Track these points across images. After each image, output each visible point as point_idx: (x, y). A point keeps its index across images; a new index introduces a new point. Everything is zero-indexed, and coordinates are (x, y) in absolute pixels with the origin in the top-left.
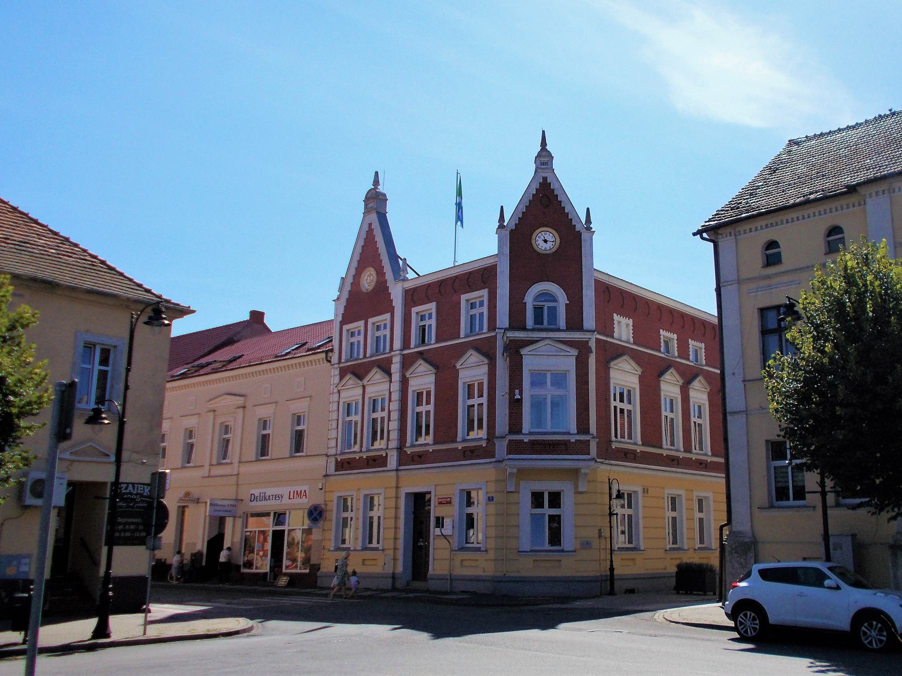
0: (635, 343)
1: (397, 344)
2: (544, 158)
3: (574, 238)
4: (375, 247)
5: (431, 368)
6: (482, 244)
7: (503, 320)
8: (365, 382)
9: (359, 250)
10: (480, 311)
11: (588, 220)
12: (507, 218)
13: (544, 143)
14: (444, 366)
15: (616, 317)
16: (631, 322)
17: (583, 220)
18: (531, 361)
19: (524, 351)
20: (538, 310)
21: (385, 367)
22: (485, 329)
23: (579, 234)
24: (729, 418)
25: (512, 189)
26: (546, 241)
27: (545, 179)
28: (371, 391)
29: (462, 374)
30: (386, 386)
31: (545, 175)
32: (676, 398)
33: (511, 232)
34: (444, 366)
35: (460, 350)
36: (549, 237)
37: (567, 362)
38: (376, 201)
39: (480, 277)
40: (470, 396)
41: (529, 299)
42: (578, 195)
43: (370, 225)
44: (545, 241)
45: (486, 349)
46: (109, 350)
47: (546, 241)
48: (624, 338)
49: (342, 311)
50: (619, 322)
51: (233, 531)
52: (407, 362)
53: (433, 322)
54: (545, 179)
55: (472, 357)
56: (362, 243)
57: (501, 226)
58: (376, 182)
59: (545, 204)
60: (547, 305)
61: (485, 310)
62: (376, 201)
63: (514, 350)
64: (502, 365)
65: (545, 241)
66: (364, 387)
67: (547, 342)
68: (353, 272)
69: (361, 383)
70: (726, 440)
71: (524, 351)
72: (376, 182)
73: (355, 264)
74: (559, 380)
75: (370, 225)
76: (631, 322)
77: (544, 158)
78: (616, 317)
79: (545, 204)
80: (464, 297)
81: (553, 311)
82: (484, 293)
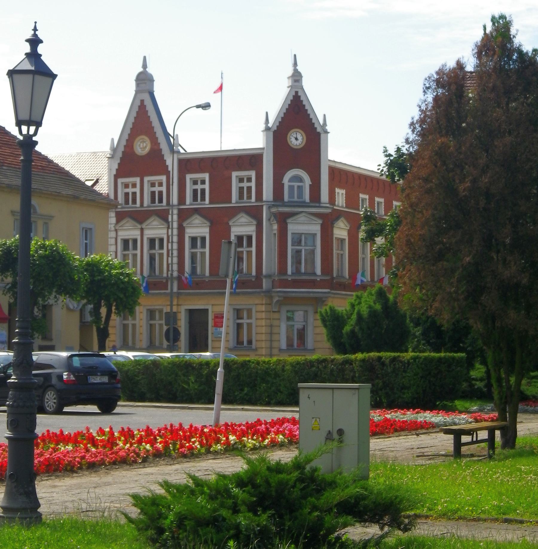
0: (346, 207)
1: (175, 200)
2: (297, 77)
3: (315, 136)
4: (144, 119)
5: (205, 221)
8: (144, 226)
11: (325, 124)
13: (295, 64)
14: (219, 222)
16: (344, 192)
17: (321, 122)
18: (294, 227)
19: (289, 221)
20: (291, 188)
21: (163, 216)
23: (319, 134)
24: (222, 149)
27: (297, 92)
28: (149, 233)
30: (165, 231)
31: (296, 90)
32: (345, 239)
33: (275, 132)
34: (219, 222)
35: (235, 211)
36: (300, 137)
37: (315, 228)
38: (144, 81)
39: (250, 160)
42: (320, 106)
44: (297, 139)
45: (255, 213)
48: (340, 205)
49: (116, 166)
50: (338, 193)
52: (184, 215)
53: (207, 187)
54: (297, 92)
55: (243, 218)
56: (134, 114)
57: (267, 129)
58: (145, 66)
59: (297, 115)
60: (296, 184)
62: (144, 81)
63: (282, 220)
65: (297, 139)
66: (142, 230)
67: (303, 214)
69: (139, 226)
70: (358, 400)
72: (145, 66)
76: (344, 192)
77: (297, 77)
79: (297, 115)
80: (235, 175)
81: (300, 188)
82: (253, 174)
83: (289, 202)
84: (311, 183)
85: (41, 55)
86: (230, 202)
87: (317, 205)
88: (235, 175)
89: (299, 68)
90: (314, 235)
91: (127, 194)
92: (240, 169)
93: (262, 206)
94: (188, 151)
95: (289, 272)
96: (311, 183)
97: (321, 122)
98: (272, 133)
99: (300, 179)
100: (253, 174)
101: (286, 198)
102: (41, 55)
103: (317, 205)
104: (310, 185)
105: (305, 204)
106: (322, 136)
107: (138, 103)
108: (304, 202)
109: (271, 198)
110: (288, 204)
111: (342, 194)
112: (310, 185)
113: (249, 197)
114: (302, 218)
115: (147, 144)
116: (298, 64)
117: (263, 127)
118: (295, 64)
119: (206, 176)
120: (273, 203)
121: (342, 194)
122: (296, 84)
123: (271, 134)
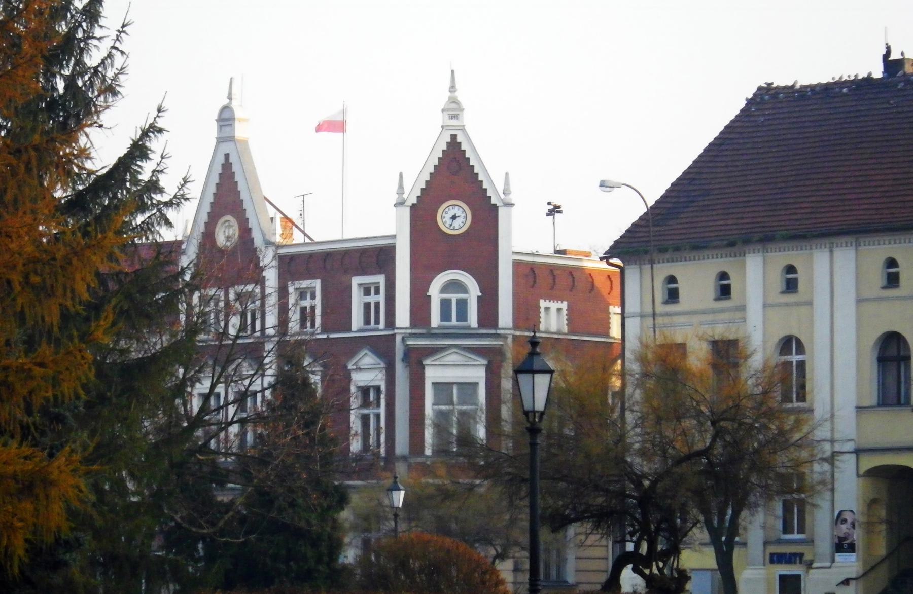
2: (454, 110)
3: (486, 214)
6: (379, 218)
7: (403, 318)
9: (212, 189)
10: (377, 300)
12: (408, 186)
13: (453, 88)
15: (543, 304)
16: (564, 305)
17: (500, 188)
18: (433, 374)
19: (427, 362)
20: (445, 305)
22: (382, 325)
23: (495, 208)
25: (417, 164)
26: (454, 218)
27: (454, 137)
29: (355, 376)
31: (454, 132)
37: (477, 373)
39: (378, 258)
40: (366, 403)
41: (435, 291)
42: (493, 165)
43: (227, 156)
45: (382, 347)
46: (772, 555)
47: (454, 218)
51: (898, 196)
53: (318, 302)
54: (454, 137)
55: (367, 359)
56: (216, 179)
57: (400, 204)
59: (455, 172)
60: (454, 297)
61: (381, 298)
63: (415, 360)
64: (401, 373)
68: (204, 218)
71: (427, 362)
73: (207, 208)
74: (468, 388)
75: (227, 156)
76: (564, 305)
77: (454, 110)
78: (543, 304)
79: (455, 172)
80: (356, 281)
81: (462, 305)
83: (439, 328)
84: (480, 294)
85: (747, 100)
86: (349, 330)
87: (493, 332)
88: (356, 281)
89: (460, 95)
90: (476, 384)
91: (303, 309)
92: (363, 272)
93: (394, 335)
94: (316, 240)
95: (428, 452)
96: (480, 294)
97: (500, 188)
98: (408, 209)
99: (454, 286)
100: (381, 279)
101: (435, 320)
102: (747, 100)
103: (493, 332)
104: (479, 297)
105: (470, 332)
106: (502, 212)
107: (221, 159)
108: (469, 328)
109: (407, 323)
110: (436, 331)
111: (559, 310)
112: (479, 297)
113: (377, 322)
114: (452, 358)
115: (234, 230)
116: (458, 86)
117: (394, 198)
118: (453, 88)
119: (317, 284)
120: (409, 331)
121: (559, 310)
122: (454, 122)
123: (406, 213)
